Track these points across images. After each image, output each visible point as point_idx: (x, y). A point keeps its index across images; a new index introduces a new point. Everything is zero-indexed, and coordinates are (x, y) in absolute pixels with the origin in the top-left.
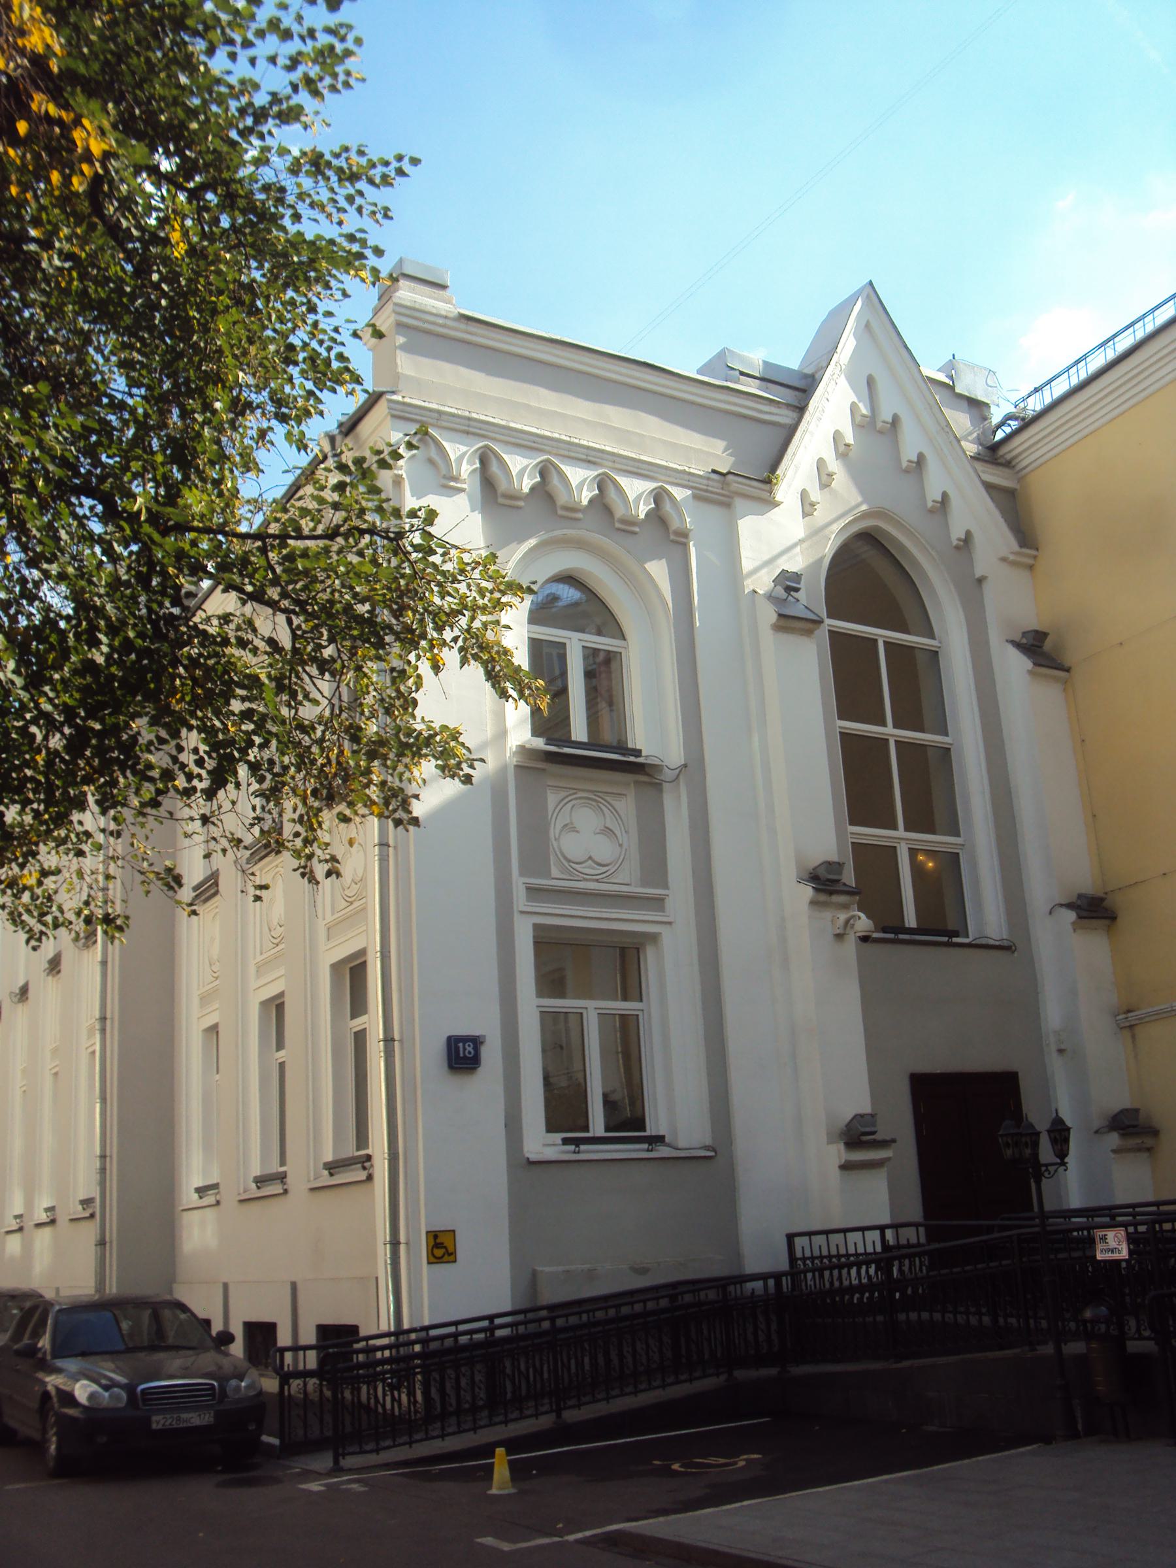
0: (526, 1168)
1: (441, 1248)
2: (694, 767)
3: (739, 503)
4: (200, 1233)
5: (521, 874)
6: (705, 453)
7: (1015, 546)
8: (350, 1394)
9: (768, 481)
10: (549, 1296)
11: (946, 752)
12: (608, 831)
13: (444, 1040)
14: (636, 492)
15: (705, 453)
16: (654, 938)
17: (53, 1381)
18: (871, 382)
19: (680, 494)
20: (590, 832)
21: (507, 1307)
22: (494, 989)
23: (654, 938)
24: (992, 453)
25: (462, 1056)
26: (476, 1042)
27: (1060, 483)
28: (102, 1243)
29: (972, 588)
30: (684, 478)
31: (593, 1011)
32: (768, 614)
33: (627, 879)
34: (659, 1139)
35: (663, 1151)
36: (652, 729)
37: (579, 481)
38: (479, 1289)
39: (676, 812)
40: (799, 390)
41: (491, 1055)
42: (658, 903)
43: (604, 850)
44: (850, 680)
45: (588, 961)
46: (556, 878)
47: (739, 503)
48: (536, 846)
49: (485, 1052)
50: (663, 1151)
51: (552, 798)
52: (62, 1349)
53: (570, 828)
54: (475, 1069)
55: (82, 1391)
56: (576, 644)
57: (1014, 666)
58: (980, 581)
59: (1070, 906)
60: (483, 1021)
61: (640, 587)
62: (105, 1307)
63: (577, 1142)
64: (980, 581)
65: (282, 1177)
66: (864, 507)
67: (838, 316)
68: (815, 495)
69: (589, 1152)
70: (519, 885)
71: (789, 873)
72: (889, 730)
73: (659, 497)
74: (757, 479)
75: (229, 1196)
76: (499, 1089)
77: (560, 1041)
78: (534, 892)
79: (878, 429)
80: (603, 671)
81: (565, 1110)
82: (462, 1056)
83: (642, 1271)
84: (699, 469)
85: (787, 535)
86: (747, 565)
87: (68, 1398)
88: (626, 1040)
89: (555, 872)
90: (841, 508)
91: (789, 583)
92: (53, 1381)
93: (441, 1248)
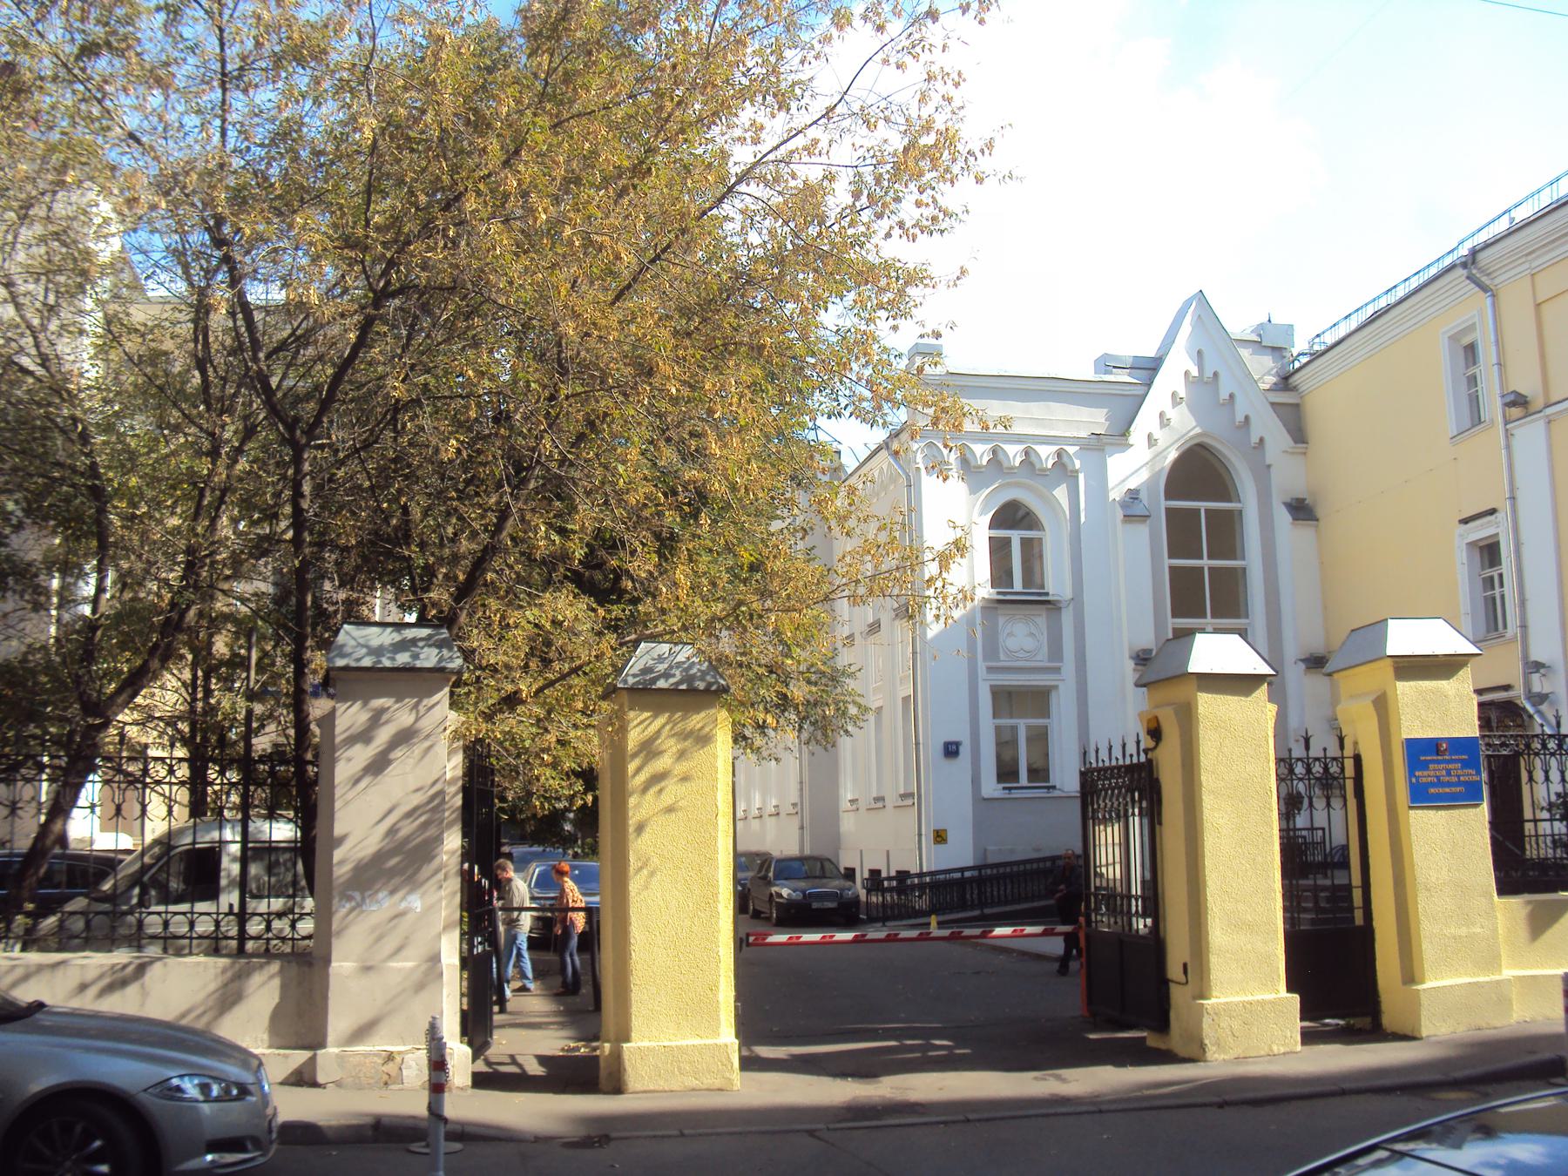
0: (981, 802)
1: (940, 837)
2: (1077, 599)
3: (1108, 448)
4: (848, 824)
5: (985, 659)
6: (1094, 419)
7: (1291, 443)
8: (900, 896)
9: (1125, 433)
10: (991, 860)
11: (1244, 569)
12: (1032, 634)
13: (1307, 1048)
14: (1046, 453)
15: (1094, 419)
16: (1056, 687)
17: (774, 889)
18: (1199, 353)
19: (1071, 450)
20: (1022, 637)
21: (971, 863)
22: (966, 717)
23: (1056, 687)
24: (1285, 382)
25: (951, 750)
26: (957, 744)
27: (1326, 398)
28: (802, 828)
29: (1263, 472)
30: (1074, 441)
31: (1022, 725)
32: (1120, 514)
33: (1042, 659)
34: (1054, 787)
35: (1056, 793)
36: (1057, 582)
37: (1014, 452)
38: (959, 854)
39: (1067, 618)
40: (1149, 368)
41: (965, 751)
42: (1057, 670)
43: (1029, 644)
44: (1181, 532)
45: (1021, 700)
46: (1004, 660)
47: (1108, 448)
48: (992, 649)
49: (961, 749)
50: (1056, 793)
51: (1001, 620)
52: (777, 877)
53: (1010, 634)
54: (1199, 445)
55: (785, 892)
56: (1015, 536)
57: (1283, 517)
58: (1269, 466)
59: (1302, 660)
60: (961, 734)
61: (1053, 504)
62: (802, 859)
63: (1010, 789)
64: (1269, 466)
65: (882, 799)
66: (1198, 430)
67: (1187, 304)
68: (1158, 434)
69: (1016, 794)
70: (982, 666)
71: (1127, 655)
72: (1205, 562)
73: (1059, 454)
74: (1120, 434)
75: (862, 805)
76: (969, 766)
77: (1005, 743)
78: (990, 669)
79: (1204, 385)
80: (1032, 550)
81: (1006, 773)
82: (951, 750)
83: (1038, 850)
84: (1084, 434)
85: (1136, 466)
86: (1110, 485)
87: (780, 896)
88: (1040, 738)
89: (1002, 657)
90: (1185, 426)
91: (1133, 495)
92: (774, 889)
93: (940, 837)
